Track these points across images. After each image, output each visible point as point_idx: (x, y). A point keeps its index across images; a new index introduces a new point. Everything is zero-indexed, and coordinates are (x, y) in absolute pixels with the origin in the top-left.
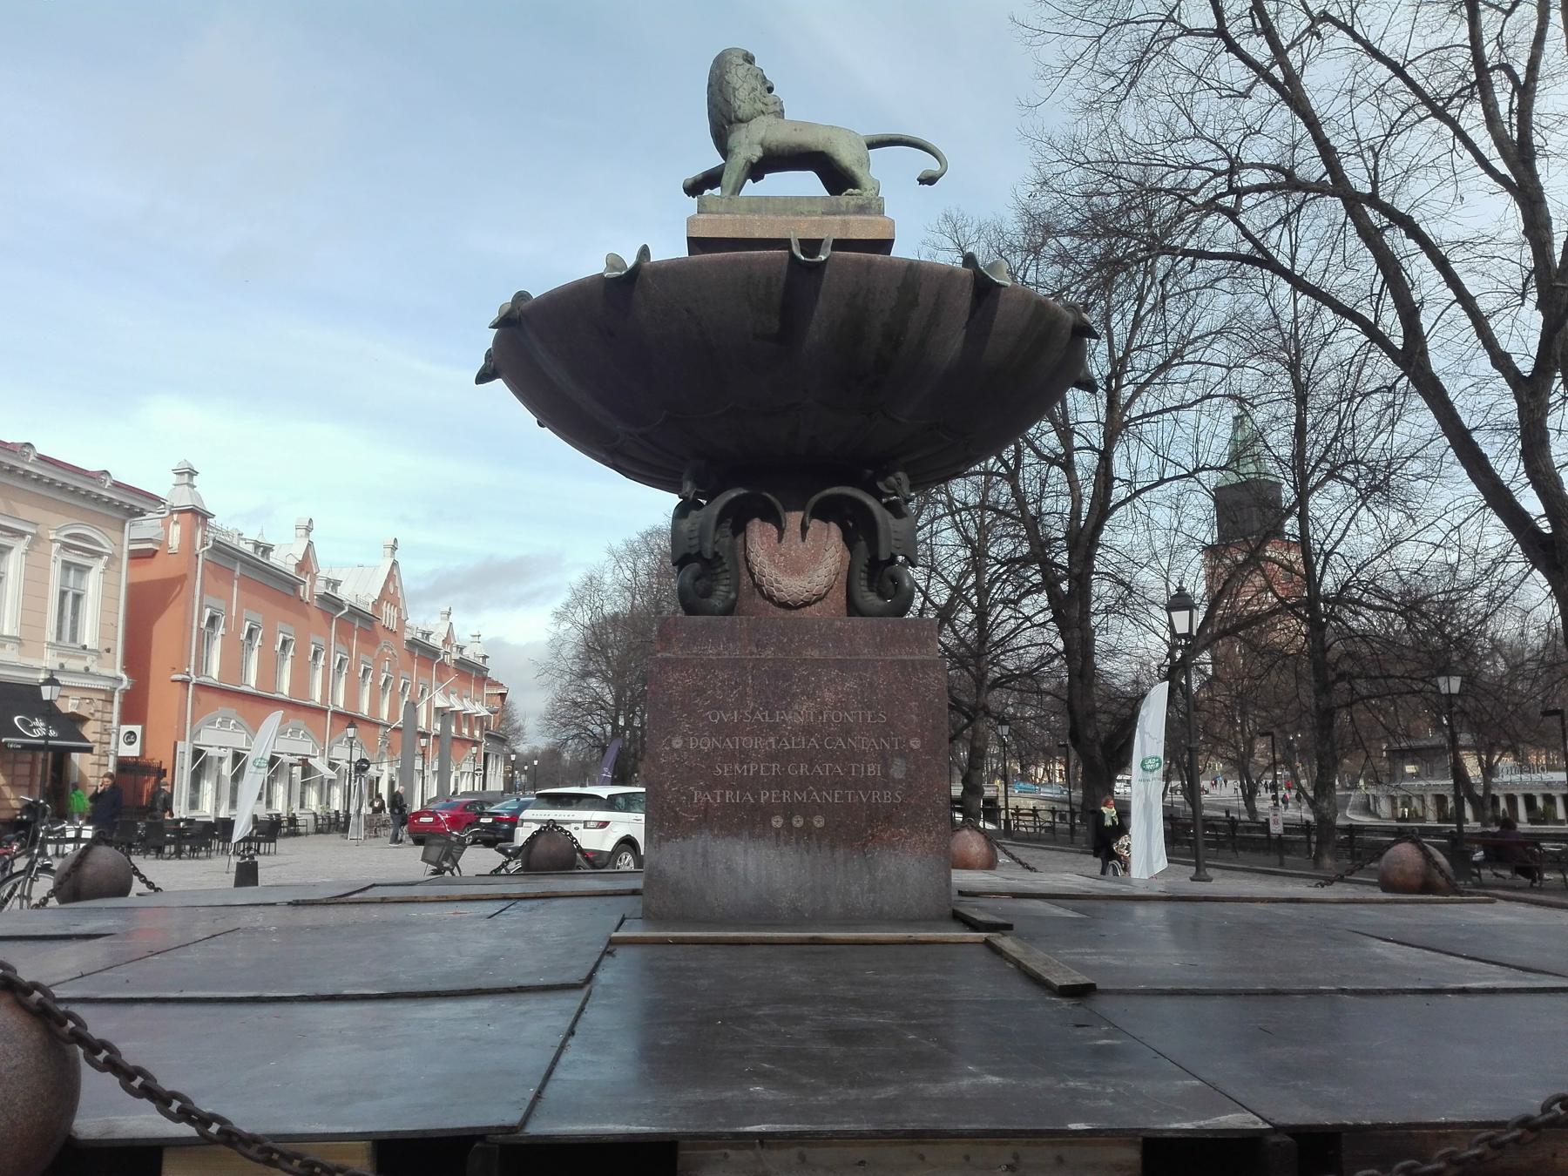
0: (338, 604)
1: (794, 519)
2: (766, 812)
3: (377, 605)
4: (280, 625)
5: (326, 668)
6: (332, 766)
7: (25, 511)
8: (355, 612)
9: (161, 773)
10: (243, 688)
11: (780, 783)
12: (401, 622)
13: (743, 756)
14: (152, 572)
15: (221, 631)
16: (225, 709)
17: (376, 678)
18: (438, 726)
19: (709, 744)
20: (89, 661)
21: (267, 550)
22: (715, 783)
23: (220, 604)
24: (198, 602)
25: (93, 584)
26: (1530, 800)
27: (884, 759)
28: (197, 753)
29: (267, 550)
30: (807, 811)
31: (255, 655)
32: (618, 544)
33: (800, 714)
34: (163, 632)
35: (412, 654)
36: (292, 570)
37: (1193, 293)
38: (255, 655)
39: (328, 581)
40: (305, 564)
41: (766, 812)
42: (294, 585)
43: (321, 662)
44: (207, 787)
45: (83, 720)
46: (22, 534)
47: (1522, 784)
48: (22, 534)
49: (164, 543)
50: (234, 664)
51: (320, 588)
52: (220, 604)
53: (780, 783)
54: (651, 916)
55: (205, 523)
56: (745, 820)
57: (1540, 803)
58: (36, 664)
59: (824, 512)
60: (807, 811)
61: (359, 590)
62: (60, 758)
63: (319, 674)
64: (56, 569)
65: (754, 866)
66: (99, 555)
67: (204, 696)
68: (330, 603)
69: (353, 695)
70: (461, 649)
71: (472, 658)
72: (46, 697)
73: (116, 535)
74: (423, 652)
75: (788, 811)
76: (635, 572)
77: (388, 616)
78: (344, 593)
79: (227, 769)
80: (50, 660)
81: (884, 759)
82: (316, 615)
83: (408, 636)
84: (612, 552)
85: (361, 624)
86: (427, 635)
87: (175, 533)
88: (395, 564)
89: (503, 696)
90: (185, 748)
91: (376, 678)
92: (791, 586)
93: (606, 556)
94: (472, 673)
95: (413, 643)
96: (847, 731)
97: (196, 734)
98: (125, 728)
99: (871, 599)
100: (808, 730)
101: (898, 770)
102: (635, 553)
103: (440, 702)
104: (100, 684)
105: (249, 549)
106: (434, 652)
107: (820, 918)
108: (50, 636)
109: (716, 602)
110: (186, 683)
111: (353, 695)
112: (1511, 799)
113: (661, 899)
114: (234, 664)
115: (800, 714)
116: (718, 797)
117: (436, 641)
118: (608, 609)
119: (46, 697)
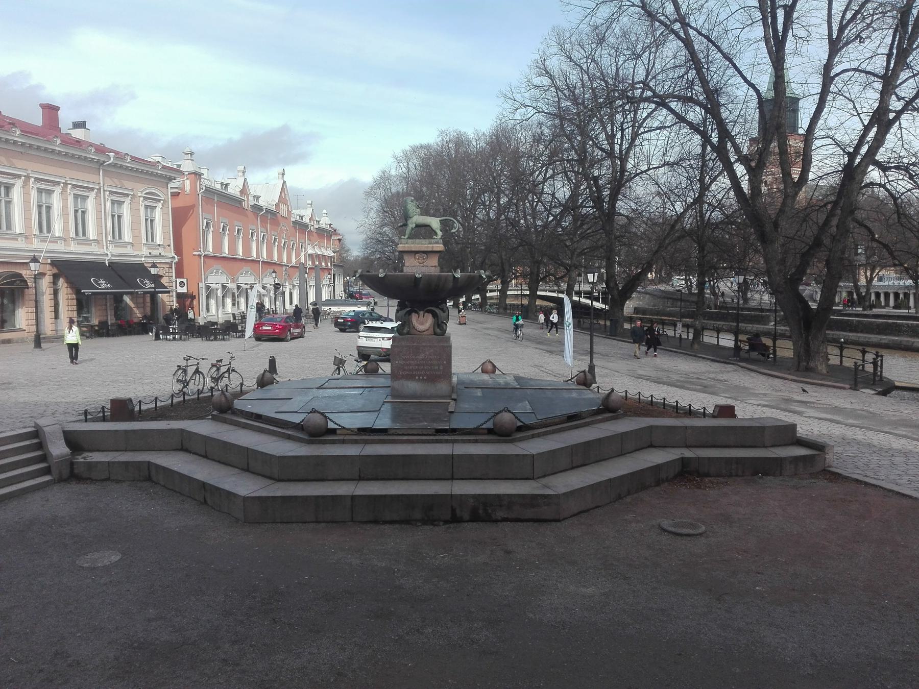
0: (260, 208)
1: (421, 313)
2: (415, 376)
3: (277, 205)
4: (236, 223)
5: (257, 241)
6: (264, 288)
7: (127, 184)
8: (268, 211)
9: (193, 297)
10: (223, 255)
11: (417, 370)
12: (289, 212)
13: (410, 365)
14: (181, 202)
15: (212, 229)
16: (217, 265)
17: (280, 242)
18: (310, 263)
19: (403, 362)
20: (161, 250)
21: (227, 185)
22: (404, 370)
23: (209, 216)
24: (201, 215)
25: (158, 214)
26: (897, 295)
27: (439, 365)
28: (208, 287)
29: (227, 185)
30: (423, 376)
31: (226, 237)
32: (399, 153)
33: (422, 356)
34: (186, 230)
35: (295, 228)
36: (238, 194)
37: (649, 93)
38: (226, 237)
39: (254, 197)
40: (244, 191)
41: (415, 376)
42: (240, 202)
43: (255, 238)
44: (213, 302)
45: (161, 277)
46: (128, 195)
47: (893, 287)
48: (128, 195)
49: (183, 189)
50: (218, 245)
51: (252, 201)
52: (209, 216)
53: (417, 370)
54: (393, 396)
55: (200, 178)
56: (410, 377)
57: (901, 296)
58: (140, 253)
59: (428, 311)
60: (423, 376)
61: (268, 199)
62: (153, 296)
63: (254, 244)
64: (142, 209)
65: (412, 386)
66: (159, 201)
67: (208, 261)
68: (257, 208)
69: (270, 252)
70: (318, 222)
71: (324, 226)
72: (153, 273)
73: (164, 190)
74: (301, 227)
75: (419, 376)
76: (408, 168)
77: (283, 210)
78: (261, 203)
79: (219, 293)
80: (145, 251)
81: (439, 365)
82: (251, 215)
83: (293, 220)
84: (395, 157)
85: (270, 217)
86: (301, 217)
87: (187, 183)
88: (284, 182)
89: (340, 240)
90: (202, 285)
91: (280, 242)
92: (421, 328)
93: (392, 160)
94: (326, 234)
95: (295, 223)
96: (431, 360)
97: (206, 279)
98: (179, 280)
99: (438, 331)
100: (423, 360)
101: (441, 368)
102: (407, 157)
103: (310, 252)
104: (166, 261)
105: (218, 187)
106: (306, 226)
107: (421, 397)
108: (144, 241)
109: (405, 331)
110: (200, 256)
111: (270, 252)
112: (878, 295)
113: (395, 394)
114: (218, 245)
115: (422, 356)
116: (405, 373)
117: (306, 220)
118: (394, 190)
119: (153, 273)
